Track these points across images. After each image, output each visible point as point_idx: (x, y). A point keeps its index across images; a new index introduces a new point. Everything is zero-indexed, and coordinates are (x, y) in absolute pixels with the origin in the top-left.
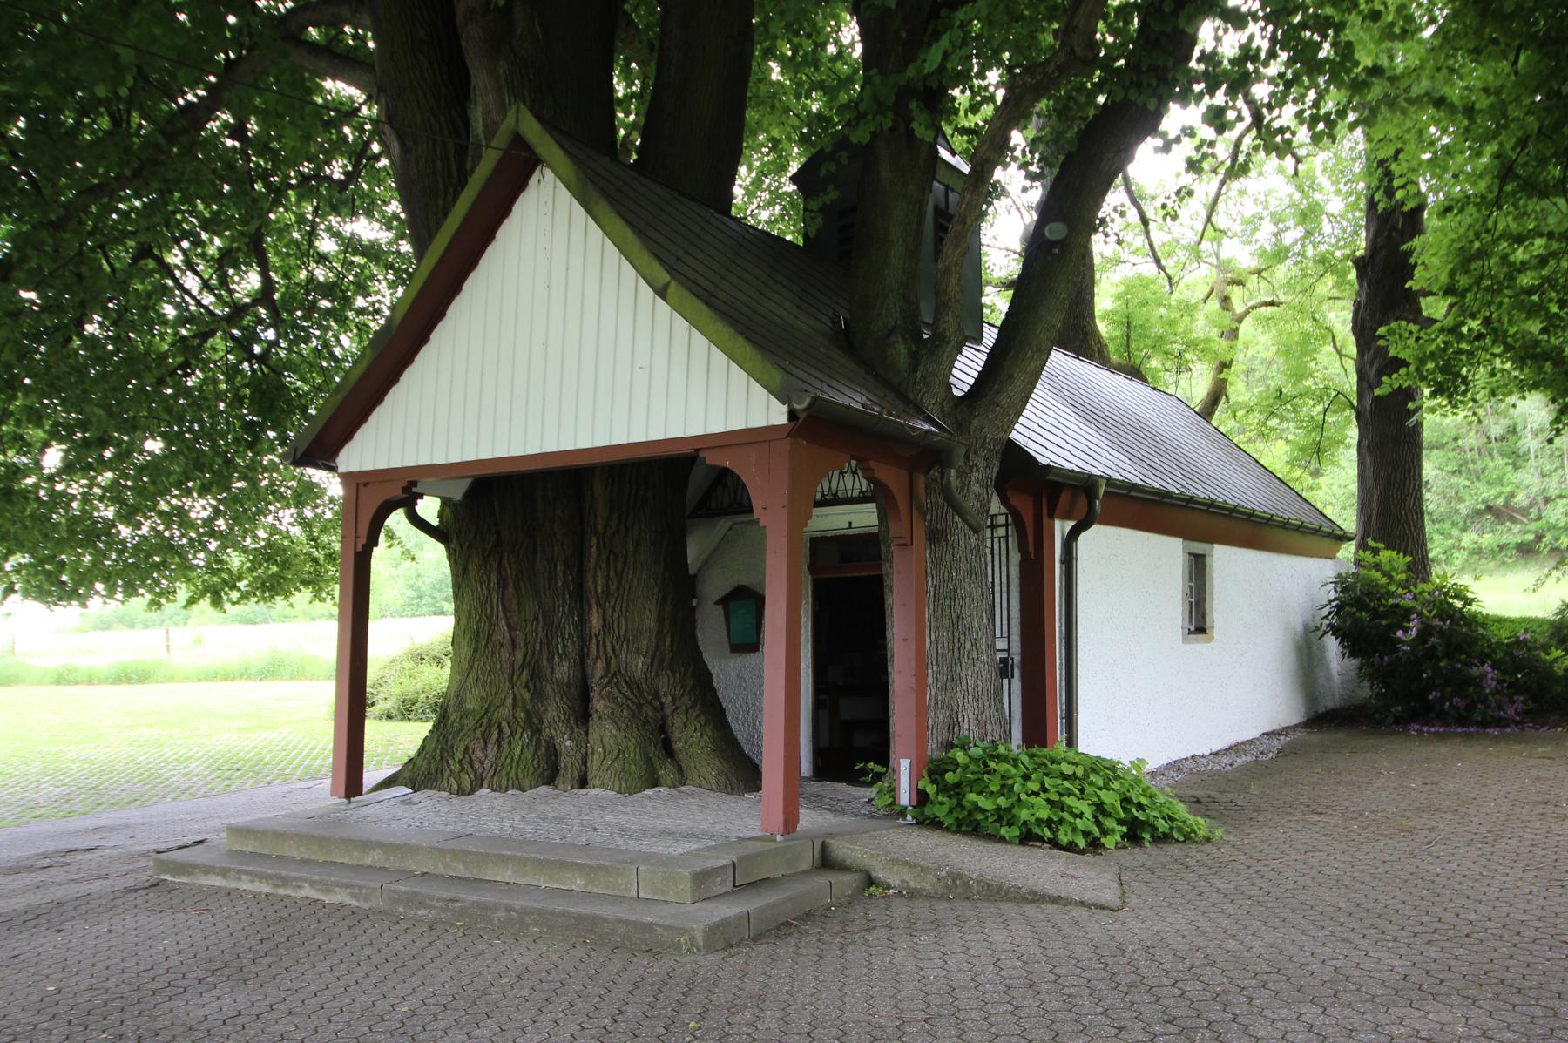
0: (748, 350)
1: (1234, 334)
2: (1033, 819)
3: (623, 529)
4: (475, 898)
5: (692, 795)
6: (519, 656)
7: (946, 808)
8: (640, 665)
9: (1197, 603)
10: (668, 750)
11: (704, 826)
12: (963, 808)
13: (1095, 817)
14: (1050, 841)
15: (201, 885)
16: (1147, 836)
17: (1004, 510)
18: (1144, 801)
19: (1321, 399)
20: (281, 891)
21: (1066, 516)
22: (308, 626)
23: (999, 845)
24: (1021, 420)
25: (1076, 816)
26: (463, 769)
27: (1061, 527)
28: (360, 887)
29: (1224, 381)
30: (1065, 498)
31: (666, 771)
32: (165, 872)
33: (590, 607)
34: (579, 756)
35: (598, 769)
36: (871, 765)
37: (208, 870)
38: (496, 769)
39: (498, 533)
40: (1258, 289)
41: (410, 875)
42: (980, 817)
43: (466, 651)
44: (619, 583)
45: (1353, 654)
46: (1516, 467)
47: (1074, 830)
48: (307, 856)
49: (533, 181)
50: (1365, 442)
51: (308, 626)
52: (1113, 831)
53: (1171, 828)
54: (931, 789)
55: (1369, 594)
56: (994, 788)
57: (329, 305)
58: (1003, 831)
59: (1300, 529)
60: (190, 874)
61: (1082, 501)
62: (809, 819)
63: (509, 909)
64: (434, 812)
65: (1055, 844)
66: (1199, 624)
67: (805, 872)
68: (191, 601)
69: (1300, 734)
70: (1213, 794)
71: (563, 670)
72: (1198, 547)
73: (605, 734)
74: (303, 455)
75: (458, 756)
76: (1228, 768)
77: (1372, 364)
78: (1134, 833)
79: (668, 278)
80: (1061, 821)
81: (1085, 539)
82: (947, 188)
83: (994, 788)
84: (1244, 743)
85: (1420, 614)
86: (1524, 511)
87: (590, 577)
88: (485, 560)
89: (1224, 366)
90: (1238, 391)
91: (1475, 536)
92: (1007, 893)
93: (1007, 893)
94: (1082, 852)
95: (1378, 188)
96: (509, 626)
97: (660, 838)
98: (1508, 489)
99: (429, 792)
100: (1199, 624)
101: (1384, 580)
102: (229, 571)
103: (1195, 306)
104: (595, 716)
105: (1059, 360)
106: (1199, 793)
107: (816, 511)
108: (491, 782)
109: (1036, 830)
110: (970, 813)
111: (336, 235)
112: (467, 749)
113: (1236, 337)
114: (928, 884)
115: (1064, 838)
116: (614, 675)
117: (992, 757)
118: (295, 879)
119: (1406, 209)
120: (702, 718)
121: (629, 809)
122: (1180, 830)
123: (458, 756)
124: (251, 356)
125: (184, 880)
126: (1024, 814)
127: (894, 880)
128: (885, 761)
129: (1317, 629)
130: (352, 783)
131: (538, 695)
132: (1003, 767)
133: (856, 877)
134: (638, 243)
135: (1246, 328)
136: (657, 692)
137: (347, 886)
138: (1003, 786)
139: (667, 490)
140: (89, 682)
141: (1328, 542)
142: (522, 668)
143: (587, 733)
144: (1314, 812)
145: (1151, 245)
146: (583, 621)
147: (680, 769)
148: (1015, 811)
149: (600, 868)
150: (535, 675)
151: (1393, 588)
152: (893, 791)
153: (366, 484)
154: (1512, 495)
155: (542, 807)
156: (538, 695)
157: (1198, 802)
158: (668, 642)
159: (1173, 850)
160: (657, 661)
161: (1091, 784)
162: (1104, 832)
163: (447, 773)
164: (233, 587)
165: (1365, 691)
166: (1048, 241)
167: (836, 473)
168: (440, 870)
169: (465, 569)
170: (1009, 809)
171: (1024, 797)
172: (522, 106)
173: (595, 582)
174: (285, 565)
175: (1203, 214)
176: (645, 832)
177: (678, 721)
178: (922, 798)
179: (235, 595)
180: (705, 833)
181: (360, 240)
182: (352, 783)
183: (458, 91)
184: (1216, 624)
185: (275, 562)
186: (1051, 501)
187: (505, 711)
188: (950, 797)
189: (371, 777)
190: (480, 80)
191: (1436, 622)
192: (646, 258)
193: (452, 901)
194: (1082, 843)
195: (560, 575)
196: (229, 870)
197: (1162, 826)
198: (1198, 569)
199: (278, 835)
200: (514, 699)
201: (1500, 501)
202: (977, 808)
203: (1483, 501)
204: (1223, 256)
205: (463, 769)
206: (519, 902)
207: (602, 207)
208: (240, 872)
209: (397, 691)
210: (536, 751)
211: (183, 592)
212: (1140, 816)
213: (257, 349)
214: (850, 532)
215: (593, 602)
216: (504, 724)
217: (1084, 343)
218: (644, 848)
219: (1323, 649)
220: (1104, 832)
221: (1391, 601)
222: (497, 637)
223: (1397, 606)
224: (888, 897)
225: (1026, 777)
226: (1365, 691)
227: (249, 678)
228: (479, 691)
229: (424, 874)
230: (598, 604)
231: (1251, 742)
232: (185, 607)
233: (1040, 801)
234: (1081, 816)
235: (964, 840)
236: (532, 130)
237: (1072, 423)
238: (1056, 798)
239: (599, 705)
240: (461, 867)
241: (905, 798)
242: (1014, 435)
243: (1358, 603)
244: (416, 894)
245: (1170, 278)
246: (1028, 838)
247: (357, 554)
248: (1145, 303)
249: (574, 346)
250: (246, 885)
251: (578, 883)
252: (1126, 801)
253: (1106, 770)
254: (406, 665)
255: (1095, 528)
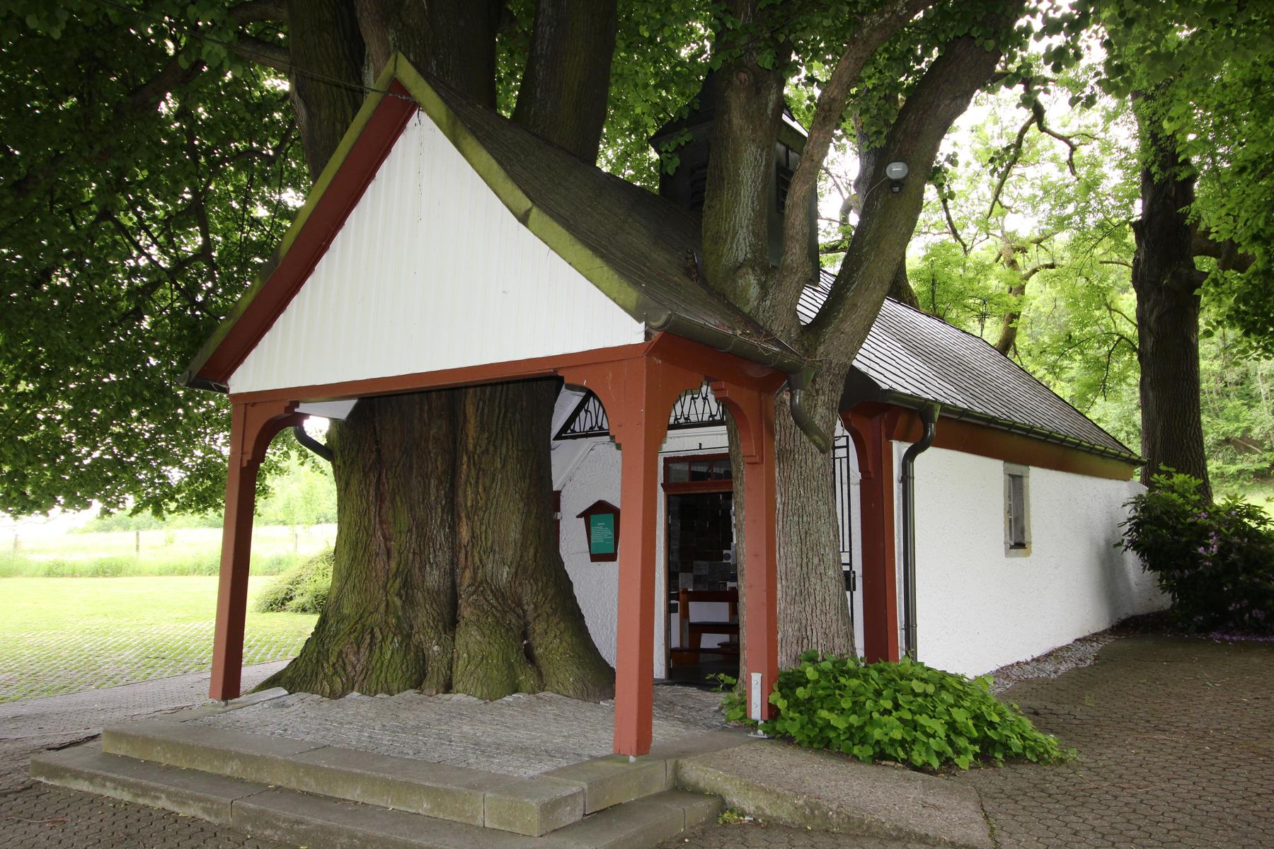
0: (606, 272)
1: (1021, 290)
2: (886, 739)
3: (491, 449)
4: (319, 821)
5: (550, 702)
6: (393, 564)
7: (797, 725)
8: (505, 573)
9: (1016, 520)
10: (529, 656)
11: (558, 740)
12: (814, 725)
13: (947, 736)
14: (904, 761)
15: (70, 790)
16: (1000, 756)
17: (846, 433)
18: (996, 719)
19: (1105, 342)
20: (141, 801)
21: (902, 439)
22: (202, 535)
23: (852, 766)
24: (864, 345)
25: (929, 736)
26: (336, 672)
27: (899, 449)
28: (212, 803)
29: (1014, 329)
30: (902, 420)
31: (526, 677)
32: (41, 774)
33: (460, 518)
34: (445, 661)
35: (463, 674)
36: (722, 676)
37: (77, 775)
38: (367, 672)
39: (378, 451)
40: (1038, 256)
41: (262, 788)
42: (832, 735)
43: (345, 559)
44: (488, 499)
45: (1153, 567)
46: (1250, 407)
47: (928, 749)
48: (172, 763)
49: (410, 124)
50: (1148, 380)
51: (202, 535)
52: (966, 750)
53: (1025, 748)
54: (782, 704)
55: (1167, 513)
56: (846, 704)
57: (260, 261)
58: (856, 750)
59: (1103, 454)
60: (62, 778)
61: (919, 423)
62: (663, 731)
63: (352, 836)
64: (304, 716)
65: (908, 764)
66: (1019, 543)
67: (659, 796)
68: (136, 511)
69: (1110, 640)
70: (1050, 706)
71: (434, 578)
72: (1017, 469)
73: (470, 639)
74: (198, 376)
75: (333, 659)
76: (1053, 676)
77: (1152, 312)
78: (988, 750)
79: (529, 204)
80: (914, 741)
81: (921, 460)
82: (788, 148)
83: (846, 704)
84: (1061, 649)
85: (1218, 532)
86: (1260, 444)
87: (460, 493)
88: (366, 475)
89: (1014, 316)
90: (1022, 341)
91: (1220, 463)
92: (869, 827)
93: (869, 827)
94: (934, 773)
95: (1153, 163)
96: (384, 537)
97: (521, 747)
98: (1245, 425)
99: (302, 695)
100: (1019, 543)
101: (1181, 501)
102: (169, 485)
103: (990, 267)
104: (462, 622)
105: (889, 306)
106: (1036, 704)
107: (670, 433)
108: (361, 685)
109: (890, 751)
110: (821, 730)
111: (267, 203)
112: (341, 652)
113: (1023, 293)
114: (784, 812)
115: (918, 759)
116: (481, 583)
117: (843, 673)
118: (156, 789)
119: (1179, 179)
120: (562, 625)
121: (487, 718)
122: (1033, 750)
123: (333, 659)
124: (193, 302)
125: (56, 783)
126: (877, 734)
127: (749, 806)
128: (735, 673)
129: (1120, 544)
130: (230, 684)
131: (409, 601)
132: (854, 683)
133: (711, 802)
134: (502, 173)
135: (1032, 286)
136: (520, 600)
137: (199, 800)
138: (855, 703)
139: (520, 401)
140: (73, 575)
141: (1123, 467)
142: (395, 576)
143: (454, 639)
144: (1157, 729)
145: (949, 218)
146: (454, 529)
147: (540, 674)
148: (867, 729)
149: (448, 792)
150: (407, 584)
151: (1189, 508)
152: (744, 703)
153: (253, 405)
154: (1249, 429)
155: (403, 715)
156: (409, 601)
157: (1036, 713)
158: (532, 552)
159: (1029, 772)
160: (519, 570)
161: (942, 701)
162: (958, 752)
163: (320, 677)
164: (172, 499)
165: (1165, 601)
166: (890, 180)
167: (689, 397)
168: (293, 785)
169: (347, 484)
170: (861, 728)
171: (876, 715)
172: (400, 54)
173: (465, 497)
174: (215, 480)
175: (989, 195)
176: (498, 746)
177: (539, 627)
178: (772, 713)
179: (173, 506)
180: (558, 750)
181: (286, 206)
182: (230, 684)
183: (356, 57)
184: (1033, 540)
185: (209, 478)
186: (890, 422)
187: (378, 617)
188: (800, 712)
189: (251, 674)
190: (373, 47)
191: (1236, 540)
192: (509, 187)
193: (299, 822)
194: (936, 764)
195: (433, 491)
196: (96, 776)
197: (1016, 743)
198: (1016, 489)
199: (148, 741)
200: (387, 605)
201: (1238, 434)
202: (829, 726)
203: (1223, 434)
204: (1007, 229)
205: (336, 672)
206: (362, 829)
207: (470, 142)
208: (105, 779)
209: (312, 588)
210: (405, 656)
211: (131, 501)
212: (991, 733)
213: (200, 298)
214: (700, 453)
215: (463, 515)
216: (377, 630)
217: (900, 292)
218: (494, 769)
219: (1122, 562)
220: (958, 752)
221: (1189, 520)
222: (374, 548)
223: (1194, 524)
224: (743, 826)
225: (878, 693)
226: (1165, 601)
227: (201, 573)
228: (354, 598)
229: (277, 788)
230: (468, 517)
231: (1067, 648)
232: (131, 515)
233: (892, 720)
234: (933, 736)
235: (817, 758)
236: (408, 74)
237: (904, 357)
238: (908, 716)
239: (466, 612)
240: (312, 782)
241: (756, 712)
242: (855, 363)
243: (1158, 521)
244: (263, 812)
245: (965, 246)
246: (880, 756)
247: (242, 470)
248: (947, 264)
249: (445, 268)
250: (110, 792)
251: (424, 807)
252: (978, 718)
253: (942, 681)
254: (321, 566)
255: (931, 451)
